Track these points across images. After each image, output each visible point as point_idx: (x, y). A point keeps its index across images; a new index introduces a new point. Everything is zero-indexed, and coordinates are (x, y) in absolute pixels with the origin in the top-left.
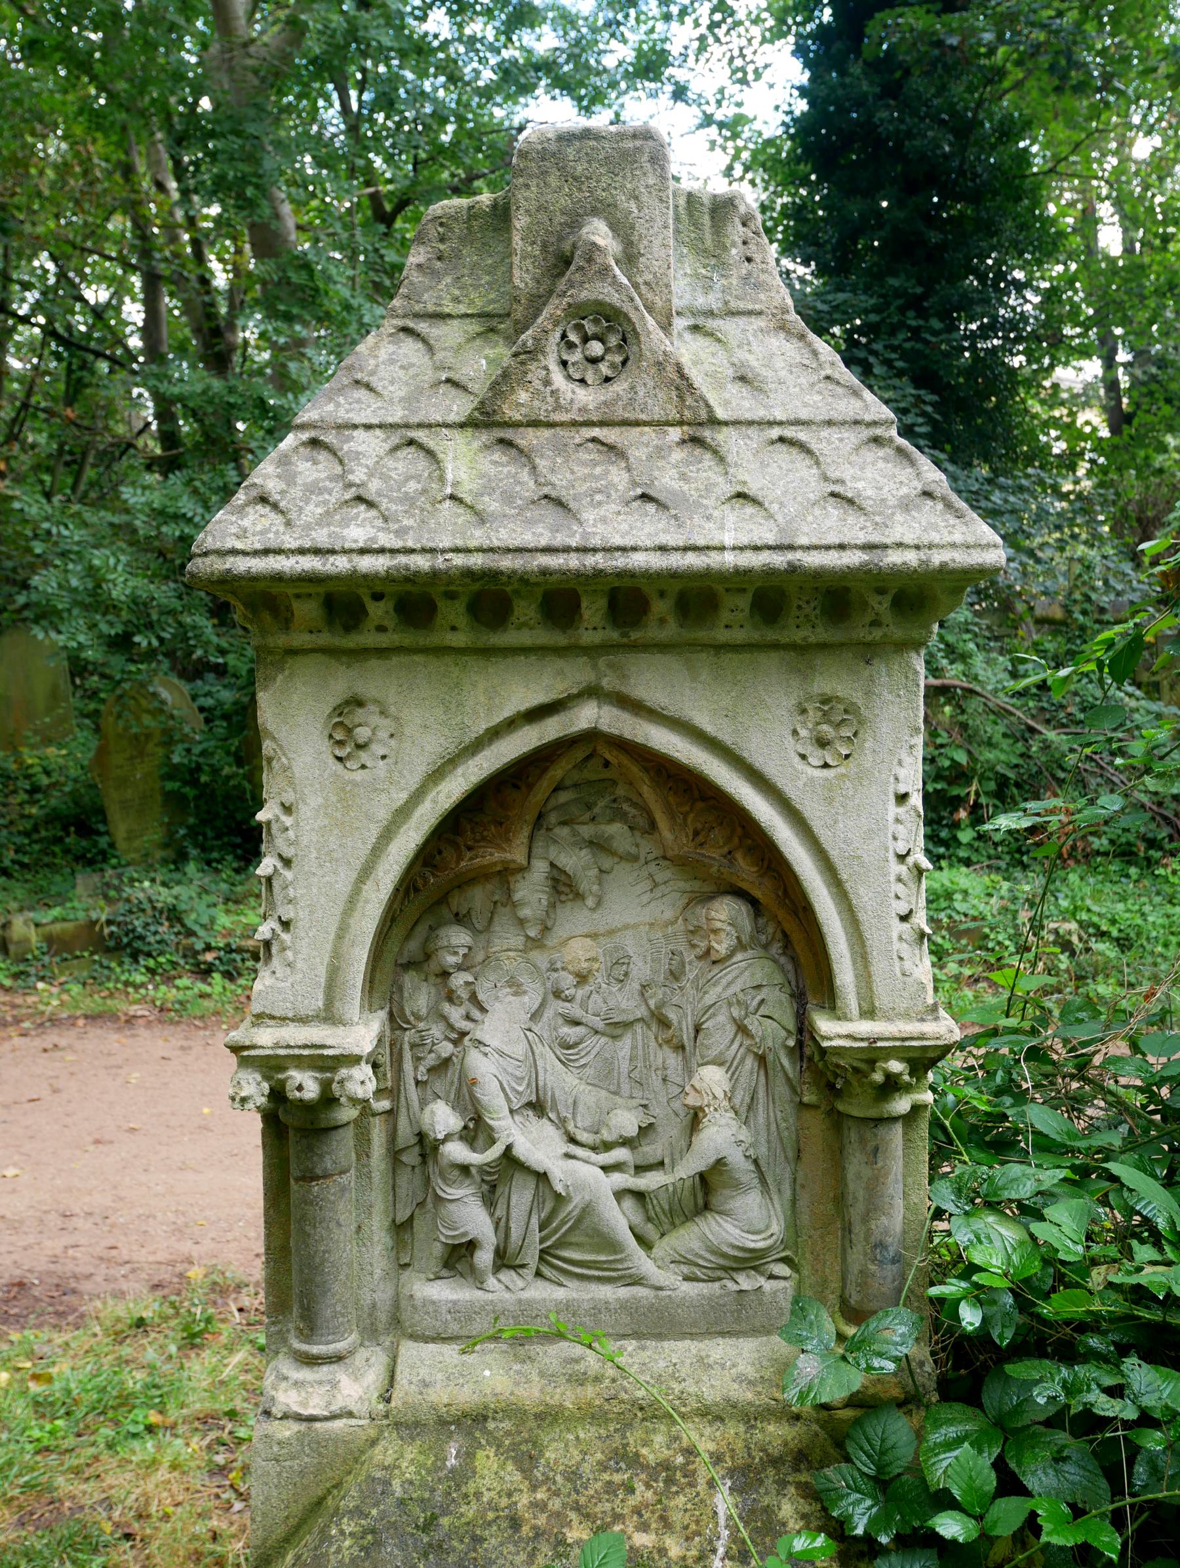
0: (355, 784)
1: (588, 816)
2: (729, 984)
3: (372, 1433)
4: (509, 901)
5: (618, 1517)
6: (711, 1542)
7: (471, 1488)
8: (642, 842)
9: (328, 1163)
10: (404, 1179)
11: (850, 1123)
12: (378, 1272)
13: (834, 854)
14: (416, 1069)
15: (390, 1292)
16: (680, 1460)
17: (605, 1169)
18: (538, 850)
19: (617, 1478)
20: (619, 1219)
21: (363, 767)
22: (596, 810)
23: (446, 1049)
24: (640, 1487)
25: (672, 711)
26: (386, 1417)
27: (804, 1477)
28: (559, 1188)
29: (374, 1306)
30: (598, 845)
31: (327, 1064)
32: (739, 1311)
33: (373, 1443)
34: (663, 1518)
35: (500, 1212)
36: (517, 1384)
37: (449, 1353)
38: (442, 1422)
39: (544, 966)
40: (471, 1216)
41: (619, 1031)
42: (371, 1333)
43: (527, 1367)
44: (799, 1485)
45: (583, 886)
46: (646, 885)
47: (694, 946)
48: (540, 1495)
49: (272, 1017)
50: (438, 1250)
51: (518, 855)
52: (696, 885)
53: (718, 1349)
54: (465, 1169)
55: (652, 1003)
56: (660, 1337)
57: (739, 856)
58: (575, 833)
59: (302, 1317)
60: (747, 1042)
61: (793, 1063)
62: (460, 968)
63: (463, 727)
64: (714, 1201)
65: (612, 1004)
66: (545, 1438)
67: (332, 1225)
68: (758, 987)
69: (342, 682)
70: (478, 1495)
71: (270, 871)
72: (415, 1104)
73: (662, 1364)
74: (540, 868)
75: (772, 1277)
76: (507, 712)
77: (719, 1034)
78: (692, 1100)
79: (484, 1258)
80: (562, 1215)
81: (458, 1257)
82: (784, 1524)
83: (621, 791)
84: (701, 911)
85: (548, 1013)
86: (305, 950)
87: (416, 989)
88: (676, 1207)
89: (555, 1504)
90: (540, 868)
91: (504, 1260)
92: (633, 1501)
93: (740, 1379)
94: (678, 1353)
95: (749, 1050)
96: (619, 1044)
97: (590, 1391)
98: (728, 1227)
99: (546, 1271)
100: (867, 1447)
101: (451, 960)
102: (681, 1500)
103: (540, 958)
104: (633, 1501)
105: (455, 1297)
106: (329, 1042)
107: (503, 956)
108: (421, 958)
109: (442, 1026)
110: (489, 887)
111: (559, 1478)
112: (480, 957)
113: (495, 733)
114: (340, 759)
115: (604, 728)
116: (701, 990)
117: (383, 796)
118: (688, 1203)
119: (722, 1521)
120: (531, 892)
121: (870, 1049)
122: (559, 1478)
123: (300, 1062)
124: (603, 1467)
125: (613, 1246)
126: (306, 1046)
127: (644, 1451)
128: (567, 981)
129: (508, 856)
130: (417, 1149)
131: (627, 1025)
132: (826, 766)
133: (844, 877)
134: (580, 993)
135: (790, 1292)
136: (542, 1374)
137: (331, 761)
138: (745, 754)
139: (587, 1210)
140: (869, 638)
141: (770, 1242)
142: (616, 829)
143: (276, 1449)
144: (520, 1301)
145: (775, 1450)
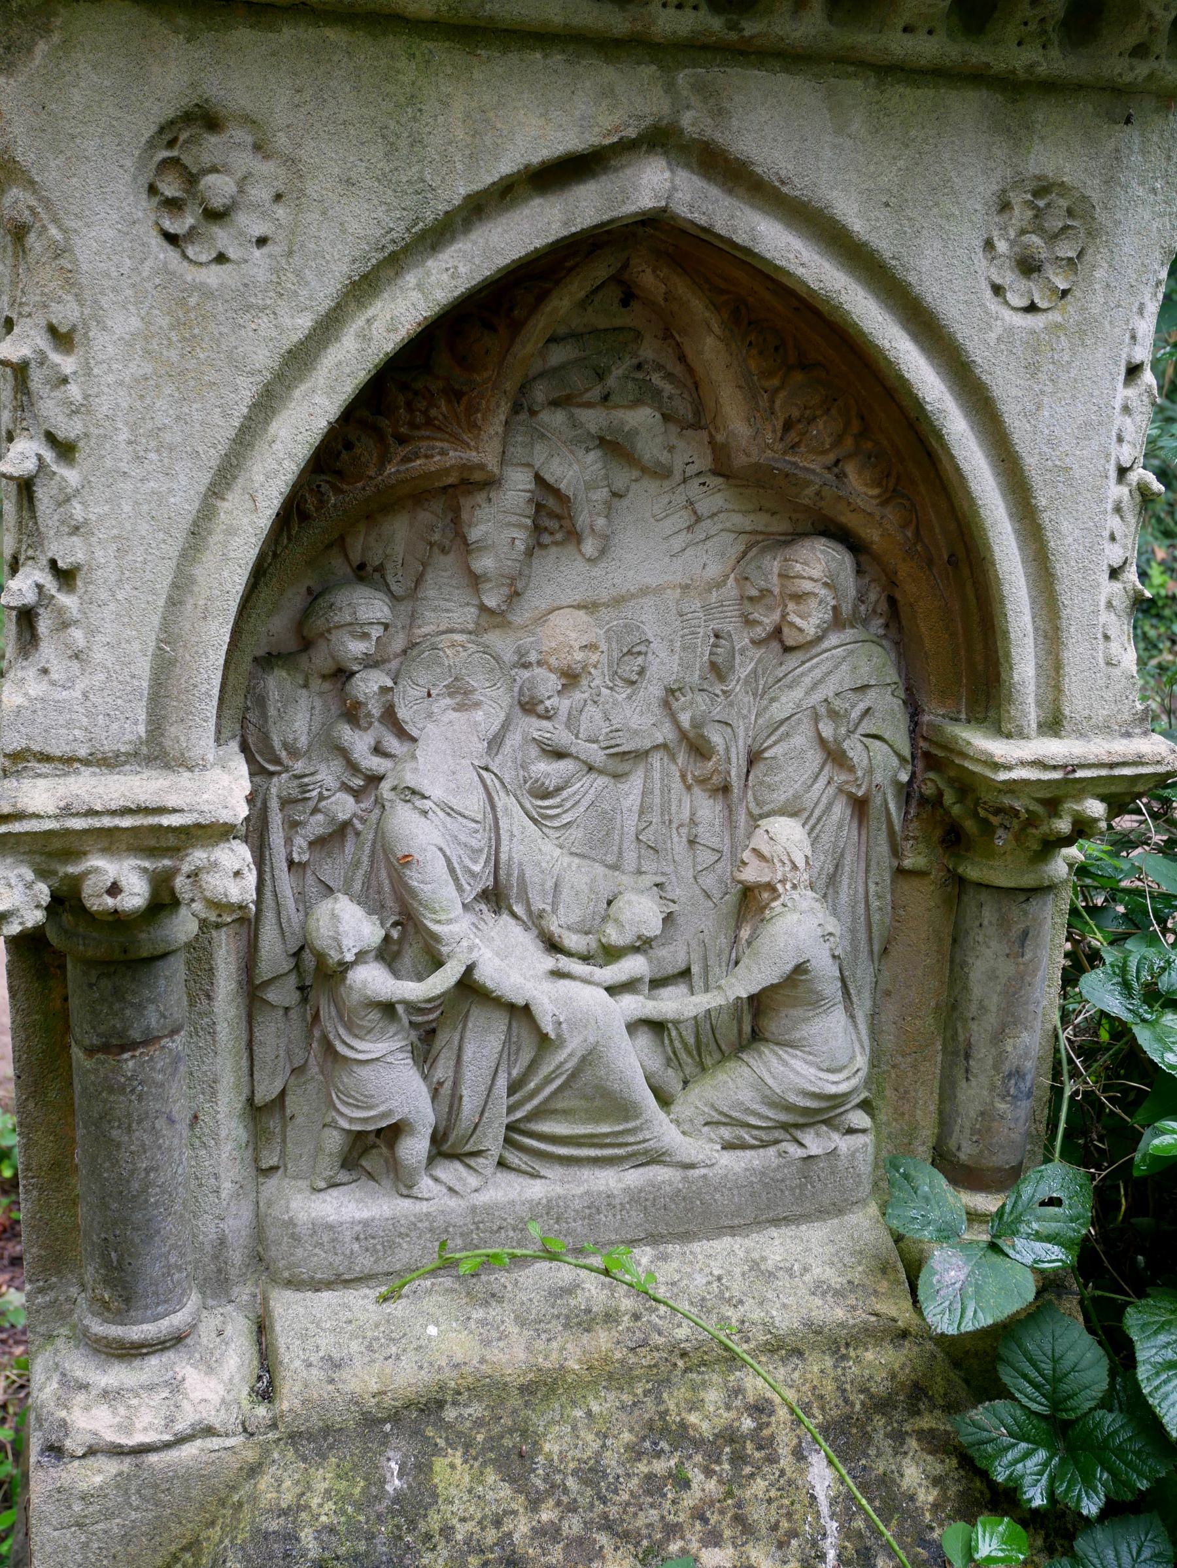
0: (207, 293)
1: (595, 393)
2: (815, 686)
3: (251, 1456)
4: (461, 543)
5: (672, 1530)
6: (814, 1544)
7: (434, 1522)
8: (681, 444)
9: (152, 1019)
10: (270, 1032)
11: (984, 896)
12: (227, 1187)
13: (1031, 462)
14: (289, 841)
15: (246, 1213)
16: (748, 1424)
17: (612, 990)
18: (517, 452)
19: (660, 1467)
20: (632, 1062)
21: (221, 258)
22: (611, 381)
23: (344, 806)
24: (696, 1476)
25: (798, 188)
26: (274, 1426)
27: (926, 1422)
28: (548, 1028)
29: (222, 1242)
30: (615, 447)
31: (165, 842)
32: (802, 1187)
33: (254, 1471)
34: (739, 1519)
35: (443, 1071)
36: (486, 1343)
37: (361, 1303)
38: (370, 1422)
39: (509, 656)
40: (392, 1083)
41: (626, 766)
42: (218, 1285)
43: (494, 1312)
44: (921, 1435)
45: (582, 519)
46: (682, 519)
47: (749, 622)
48: (547, 1515)
49: (45, 758)
50: (334, 1141)
51: (486, 454)
52: (761, 521)
53: (776, 1246)
54: (388, 1009)
55: (685, 719)
56: (686, 1237)
57: (850, 469)
58: (575, 424)
59: (107, 1282)
60: (841, 777)
61: (899, 808)
62: (371, 662)
63: (423, 189)
64: (772, 1026)
65: (617, 722)
66: (539, 1422)
67: (160, 1123)
68: (864, 688)
69: (177, 70)
70: (447, 1531)
71: (30, 466)
72: (289, 903)
73: (700, 1280)
74: (517, 487)
75: (851, 1131)
76: (506, 167)
77: (796, 767)
78: (752, 874)
79: (415, 1148)
80: (545, 1070)
81: (370, 1151)
82: (912, 1498)
83: (648, 351)
84: (774, 565)
85: (514, 739)
86: (109, 628)
87: (288, 701)
88: (706, 1037)
89: (573, 1526)
90: (517, 487)
91: (446, 1147)
92: (689, 1500)
93: (820, 1289)
94: (714, 1259)
95: (840, 790)
96: (625, 787)
97: (603, 1339)
98: (798, 1064)
99: (513, 1158)
100: (1033, 1374)
101: (357, 648)
102: (759, 1486)
103: (503, 644)
104: (689, 1500)
105: (365, 1214)
106: (172, 801)
107: (444, 641)
108: (292, 645)
109: (337, 765)
110: (424, 516)
111: (571, 1483)
112: (398, 644)
113: (478, 208)
114: (172, 239)
115: (683, 211)
116: (764, 693)
117: (264, 321)
118: (728, 1034)
119: (824, 1509)
120: (498, 525)
121: (1065, 781)
122: (571, 1483)
123: (110, 840)
124: (636, 1453)
125: (624, 1109)
126: (125, 811)
127: (693, 1418)
128: (548, 683)
129: (473, 456)
130: (292, 980)
131: (640, 756)
132: (1032, 308)
133: (1042, 502)
134: (564, 705)
135: (871, 1149)
136: (521, 1321)
137: (156, 242)
138: (912, 278)
139: (589, 1058)
140: (1128, 78)
141: (854, 1082)
142: (641, 419)
143: (77, 1507)
144: (473, 1209)
145: (880, 1387)
